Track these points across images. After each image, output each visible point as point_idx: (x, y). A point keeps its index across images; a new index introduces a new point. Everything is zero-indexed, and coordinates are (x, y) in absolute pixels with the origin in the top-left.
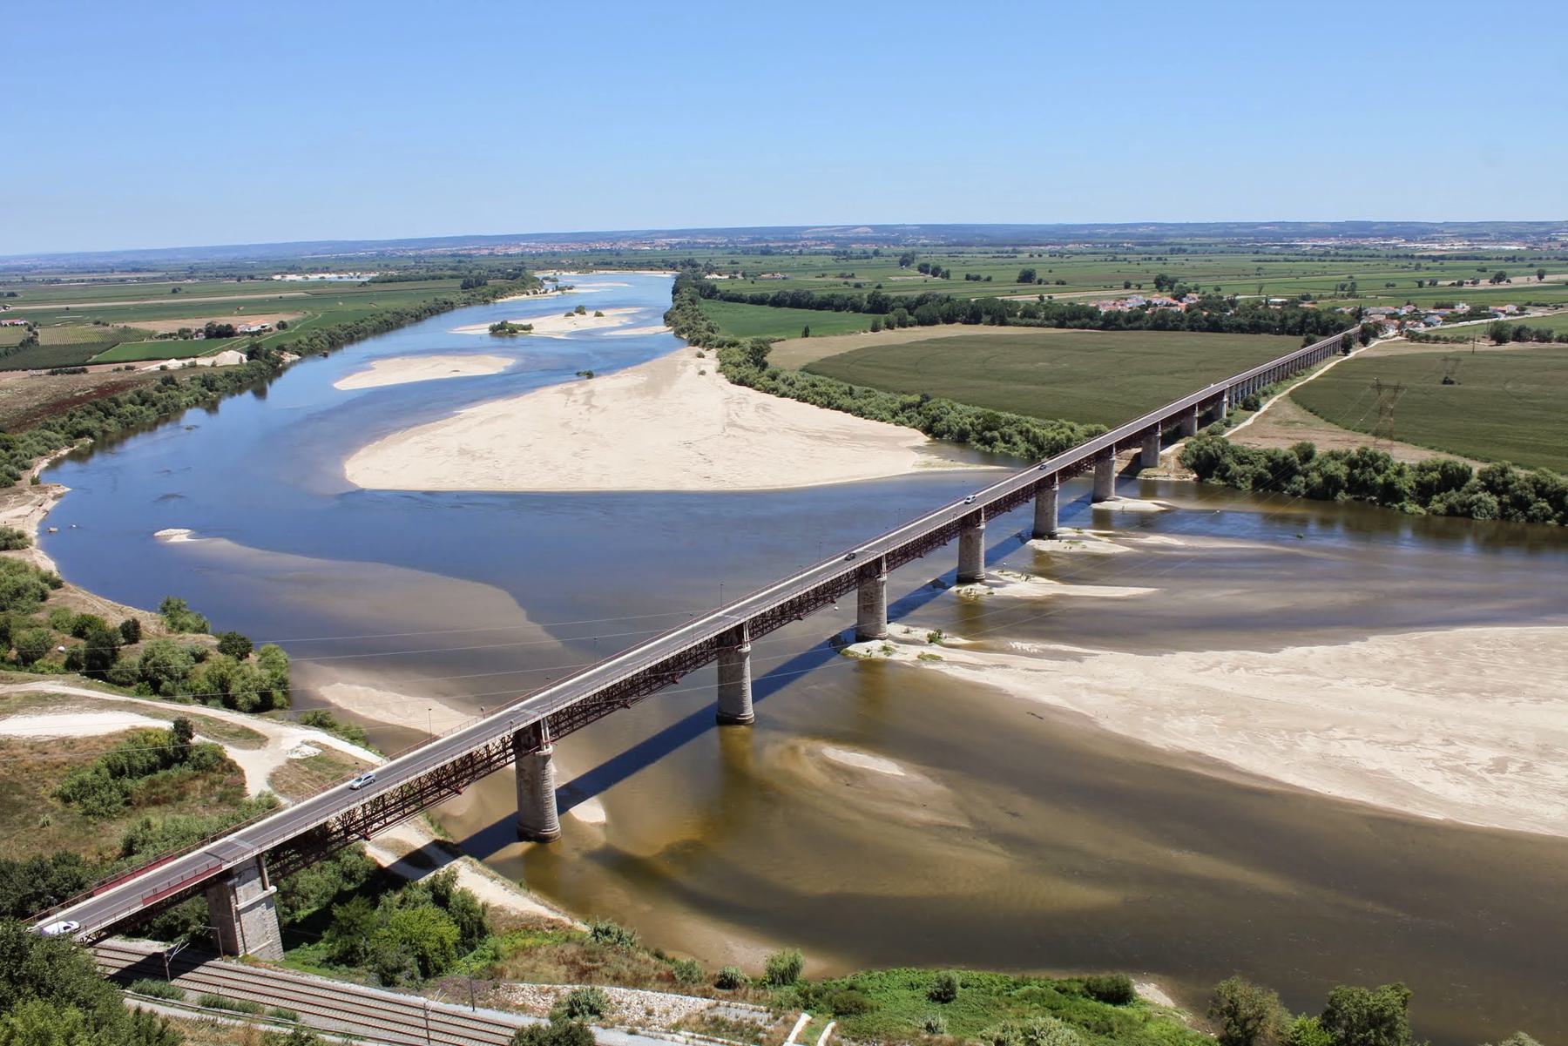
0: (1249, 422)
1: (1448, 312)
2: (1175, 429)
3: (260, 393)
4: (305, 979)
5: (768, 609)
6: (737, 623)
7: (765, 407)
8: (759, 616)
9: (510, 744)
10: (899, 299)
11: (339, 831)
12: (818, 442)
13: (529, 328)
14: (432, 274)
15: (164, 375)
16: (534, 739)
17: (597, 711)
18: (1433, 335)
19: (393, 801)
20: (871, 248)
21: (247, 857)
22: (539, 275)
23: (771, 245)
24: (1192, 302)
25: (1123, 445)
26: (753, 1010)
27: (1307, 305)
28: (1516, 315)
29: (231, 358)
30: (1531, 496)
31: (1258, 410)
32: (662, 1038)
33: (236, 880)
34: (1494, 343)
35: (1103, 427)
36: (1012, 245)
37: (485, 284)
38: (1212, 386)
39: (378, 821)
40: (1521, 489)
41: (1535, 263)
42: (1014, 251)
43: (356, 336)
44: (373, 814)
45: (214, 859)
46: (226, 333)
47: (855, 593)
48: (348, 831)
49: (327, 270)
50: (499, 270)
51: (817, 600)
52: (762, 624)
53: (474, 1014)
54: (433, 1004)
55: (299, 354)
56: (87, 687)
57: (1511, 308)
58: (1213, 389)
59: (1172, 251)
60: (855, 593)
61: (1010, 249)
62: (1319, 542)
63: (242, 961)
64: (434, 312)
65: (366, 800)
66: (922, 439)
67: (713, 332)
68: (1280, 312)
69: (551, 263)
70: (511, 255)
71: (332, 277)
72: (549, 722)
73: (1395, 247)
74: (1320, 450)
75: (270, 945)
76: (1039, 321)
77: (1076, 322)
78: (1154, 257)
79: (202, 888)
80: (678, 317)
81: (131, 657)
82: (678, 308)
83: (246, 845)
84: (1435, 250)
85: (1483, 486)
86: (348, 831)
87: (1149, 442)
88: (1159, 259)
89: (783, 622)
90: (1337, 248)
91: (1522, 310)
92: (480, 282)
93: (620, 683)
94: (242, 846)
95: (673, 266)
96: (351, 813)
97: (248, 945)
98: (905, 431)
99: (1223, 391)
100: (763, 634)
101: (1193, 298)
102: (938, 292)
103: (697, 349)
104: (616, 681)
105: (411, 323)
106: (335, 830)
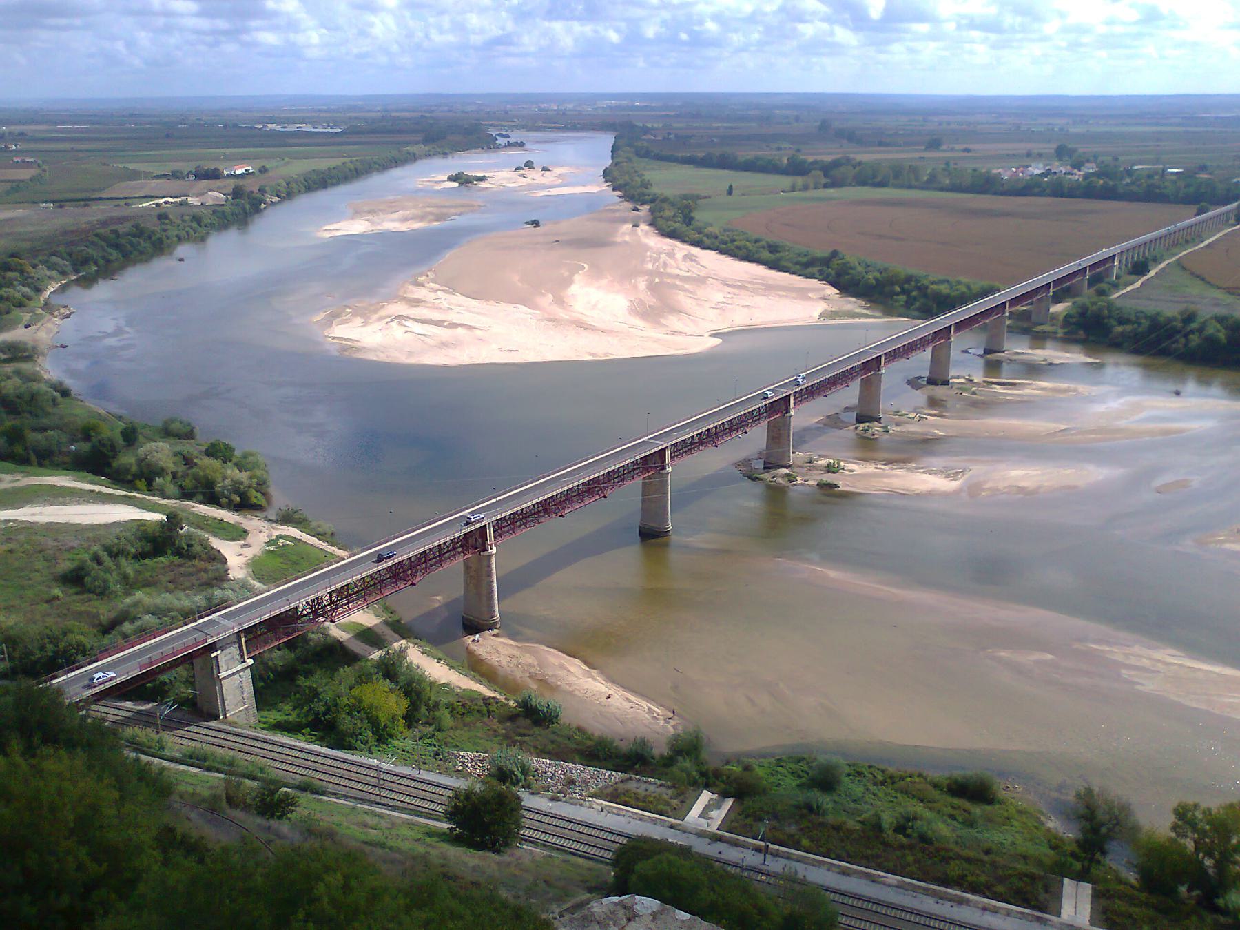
0: (1138, 284)
2: (1063, 288)
4: (276, 739)
5: (688, 436)
6: (661, 447)
7: (689, 257)
8: (680, 442)
9: (459, 544)
10: (815, 162)
11: (308, 614)
12: (736, 291)
13: (483, 179)
15: (159, 211)
19: (356, 590)
21: (228, 633)
24: (1091, 171)
26: (661, 785)
27: (1203, 176)
29: (215, 196)
32: (581, 805)
33: (219, 652)
35: (997, 284)
38: (1104, 250)
39: (342, 606)
43: (329, 181)
44: (338, 600)
45: (200, 633)
46: (214, 175)
48: (315, 613)
51: (731, 430)
52: (682, 449)
53: (419, 776)
54: (385, 766)
56: (91, 483)
58: (1105, 252)
63: (223, 722)
64: (398, 162)
65: (333, 588)
66: (831, 291)
67: (647, 188)
68: (1175, 182)
72: (494, 527)
75: (247, 709)
79: (189, 658)
80: (616, 173)
81: (127, 459)
82: (616, 165)
83: (225, 622)
86: (315, 613)
93: (557, 495)
94: (223, 625)
96: (319, 600)
97: (227, 708)
98: (814, 283)
99: (1114, 256)
101: (1091, 168)
104: (553, 493)
105: (378, 170)
106: (305, 612)
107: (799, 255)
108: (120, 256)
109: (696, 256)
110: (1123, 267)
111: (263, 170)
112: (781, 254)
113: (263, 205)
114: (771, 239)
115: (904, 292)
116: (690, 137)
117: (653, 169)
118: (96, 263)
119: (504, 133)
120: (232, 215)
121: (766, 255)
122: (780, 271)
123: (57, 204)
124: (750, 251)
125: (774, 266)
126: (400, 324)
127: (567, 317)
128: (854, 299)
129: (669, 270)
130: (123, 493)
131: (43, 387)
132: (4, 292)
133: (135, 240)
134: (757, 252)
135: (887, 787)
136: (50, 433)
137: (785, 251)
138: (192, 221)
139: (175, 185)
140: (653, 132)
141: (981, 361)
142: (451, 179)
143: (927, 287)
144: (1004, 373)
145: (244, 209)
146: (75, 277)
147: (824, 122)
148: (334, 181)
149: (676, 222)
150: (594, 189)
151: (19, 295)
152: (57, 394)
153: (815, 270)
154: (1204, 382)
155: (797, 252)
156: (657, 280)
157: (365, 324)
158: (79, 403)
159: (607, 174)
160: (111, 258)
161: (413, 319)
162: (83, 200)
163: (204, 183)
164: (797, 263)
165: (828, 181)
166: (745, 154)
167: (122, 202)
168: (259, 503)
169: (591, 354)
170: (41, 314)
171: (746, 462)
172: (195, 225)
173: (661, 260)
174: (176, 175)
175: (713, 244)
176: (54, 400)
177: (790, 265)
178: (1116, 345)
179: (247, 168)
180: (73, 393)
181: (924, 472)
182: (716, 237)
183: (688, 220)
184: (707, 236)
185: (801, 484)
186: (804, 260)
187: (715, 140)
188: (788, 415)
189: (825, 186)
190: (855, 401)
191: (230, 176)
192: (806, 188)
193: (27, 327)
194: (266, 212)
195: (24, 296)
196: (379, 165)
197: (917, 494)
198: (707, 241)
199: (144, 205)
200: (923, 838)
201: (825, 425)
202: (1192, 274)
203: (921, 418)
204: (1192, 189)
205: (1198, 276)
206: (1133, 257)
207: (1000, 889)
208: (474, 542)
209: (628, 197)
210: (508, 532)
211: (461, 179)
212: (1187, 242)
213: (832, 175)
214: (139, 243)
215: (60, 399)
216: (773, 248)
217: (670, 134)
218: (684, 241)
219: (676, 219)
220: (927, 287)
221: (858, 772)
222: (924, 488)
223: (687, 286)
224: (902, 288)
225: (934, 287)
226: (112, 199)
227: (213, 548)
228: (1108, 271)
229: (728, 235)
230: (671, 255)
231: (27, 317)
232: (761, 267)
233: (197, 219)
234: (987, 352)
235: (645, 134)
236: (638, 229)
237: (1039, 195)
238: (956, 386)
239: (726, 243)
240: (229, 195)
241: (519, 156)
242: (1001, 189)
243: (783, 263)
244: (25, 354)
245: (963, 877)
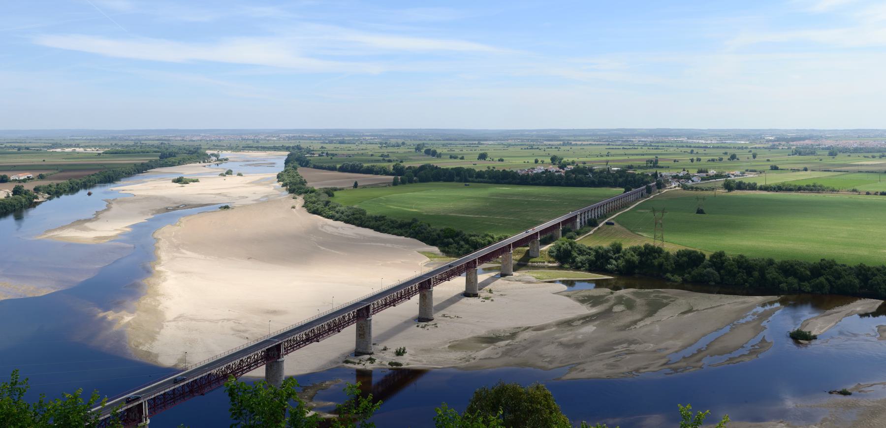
0: (591, 232)
1: (704, 175)
2: (548, 236)
3: (19, 218)
6: (277, 344)
14: (142, 150)
16: (138, 415)
17: (241, 371)
18: (695, 186)
20: (400, 141)
22: (209, 152)
23: (345, 138)
25: (516, 244)
28: (740, 176)
30: (736, 270)
31: (628, 207)
34: (727, 191)
36: (478, 140)
40: (730, 266)
41: (753, 150)
42: (479, 144)
47: (465, 273)
49: (78, 146)
50: (184, 149)
55: (49, 193)
57: (738, 172)
59: (564, 145)
60: (465, 273)
61: (477, 142)
67: (303, 185)
69: (217, 146)
70: (194, 141)
71: (81, 150)
73: (682, 142)
74: (625, 246)
76: (486, 180)
77: (505, 181)
78: (553, 147)
80: (285, 177)
84: (702, 143)
85: (709, 265)
87: (533, 243)
88: (556, 148)
89: (307, 343)
90: (651, 142)
91: (743, 174)
92: (171, 155)
95: (287, 149)
100: (294, 350)
103: (293, 195)
184: (337, 212)
191: (15, 180)
196: (126, 174)
206: (588, 217)
208: (134, 416)
210: (161, 408)
228: (574, 225)
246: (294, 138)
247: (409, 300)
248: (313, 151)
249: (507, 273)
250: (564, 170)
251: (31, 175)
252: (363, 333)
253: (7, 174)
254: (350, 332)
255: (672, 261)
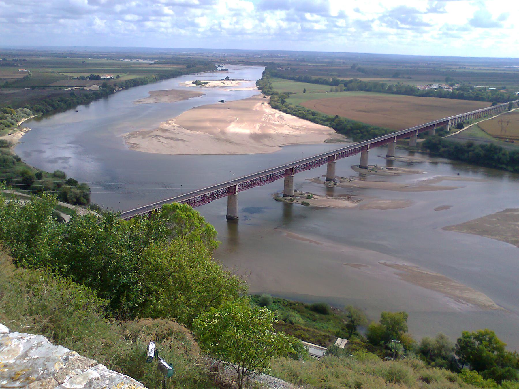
0: (458, 133)
7: (281, 117)
12: (294, 130)
13: (206, 83)
29: (95, 87)
31: (462, 129)
37: (195, 67)
38: (445, 118)
47: (360, 153)
49: (140, 58)
56: (21, 193)
60: (360, 153)
62: (139, 77)
67: (271, 89)
80: (261, 83)
102: (381, 206)
105: (165, 79)
107: (323, 117)
108: (53, 109)
109: (283, 116)
110: (453, 125)
111: (118, 77)
112: (316, 116)
113: (115, 91)
114: (313, 110)
115: (361, 132)
116: (297, 69)
117: (277, 81)
118: (42, 111)
119: (221, 65)
120: (101, 94)
121: (311, 116)
122: (315, 123)
123: (32, 88)
124: (305, 115)
125: (313, 121)
126: (157, 138)
127: (224, 138)
128: (341, 135)
129: (270, 121)
130: (19, 194)
131: (10, 157)
132: (3, 121)
133: (59, 103)
134: (307, 115)
135: (288, 307)
136: (8, 174)
137: (318, 115)
138: (84, 96)
139: (82, 82)
140: (282, 67)
141: (385, 161)
142: (193, 83)
143: (370, 131)
144: (394, 165)
145: (106, 92)
146: (33, 117)
147: (354, 65)
148: (146, 82)
149: (278, 103)
150: (251, 89)
151: (8, 123)
152: (15, 160)
153: (328, 123)
154: (475, 172)
155: (322, 115)
156: (264, 125)
157: (143, 138)
158: (23, 164)
159: (258, 83)
160: (49, 110)
161: (162, 137)
162: (42, 87)
163: (93, 82)
164: (322, 120)
165: (346, 88)
166: (314, 77)
167: (58, 88)
168: (84, 202)
169: (228, 152)
170: (16, 130)
171: (276, 194)
172: (85, 98)
173: (269, 117)
174: (83, 78)
175: (291, 111)
176: (14, 162)
177: (319, 121)
178: (441, 156)
179: (111, 76)
180: (22, 160)
181: (345, 200)
182: (292, 109)
183: (283, 102)
184: (289, 108)
185: (295, 203)
186: (324, 119)
187: (307, 70)
188: (292, 176)
189: (345, 90)
190: (325, 174)
192: (337, 91)
193: (9, 135)
194: (116, 94)
195: (10, 123)
197: (339, 208)
198: (289, 110)
199: (67, 89)
200: (291, 323)
201: (313, 182)
202: (481, 129)
203: (351, 180)
204: (494, 96)
205: (483, 130)
207: (312, 339)
209: (264, 93)
211: (197, 83)
212: (485, 117)
213: (348, 87)
214: (61, 104)
215: (16, 162)
216: (313, 114)
217: (289, 68)
218: (280, 111)
219: (278, 102)
220: (370, 131)
221: (279, 302)
222: (343, 205)
223: (275, 128)
224: (361, 131)
225: (373, 131)
226: (54, 87)
227: (61, 217)
229: (297, 109)
230: (273, 115)
231: (10, 131)
232: (308, 121)
233: (86, 96)
234: (387, 156)
235: (278, 67)
236: (263, 106)
237: (431, 96)
238: (369, 169)
239: (296, 111)
240: (101, 86)
241: (224, 75)
242: (417, 93)
243: (316, 120)
244: (6, 145)
245: (300, 335)
246: (272, 56)
247: (273, 183)
248: (282, 66)
249: (391, 155)
250: (452, 87)
251: (113, 76)
252: (288, 184)
253: (100, 75)
254: (281, 181)
255: (508, 157)
